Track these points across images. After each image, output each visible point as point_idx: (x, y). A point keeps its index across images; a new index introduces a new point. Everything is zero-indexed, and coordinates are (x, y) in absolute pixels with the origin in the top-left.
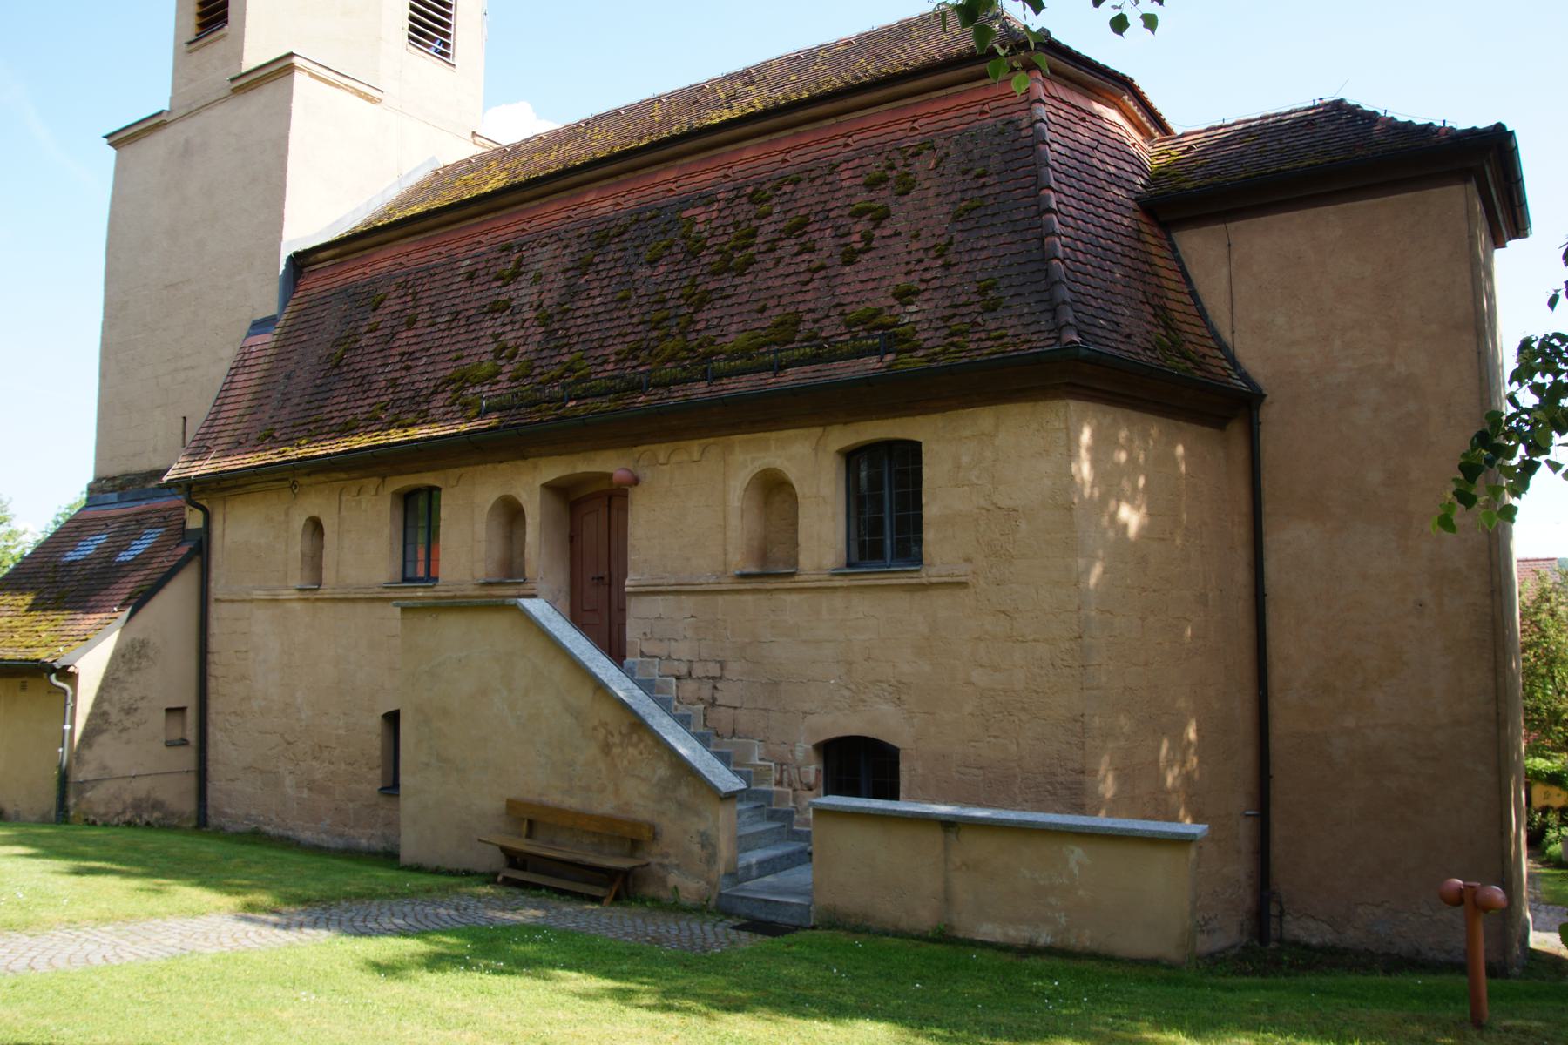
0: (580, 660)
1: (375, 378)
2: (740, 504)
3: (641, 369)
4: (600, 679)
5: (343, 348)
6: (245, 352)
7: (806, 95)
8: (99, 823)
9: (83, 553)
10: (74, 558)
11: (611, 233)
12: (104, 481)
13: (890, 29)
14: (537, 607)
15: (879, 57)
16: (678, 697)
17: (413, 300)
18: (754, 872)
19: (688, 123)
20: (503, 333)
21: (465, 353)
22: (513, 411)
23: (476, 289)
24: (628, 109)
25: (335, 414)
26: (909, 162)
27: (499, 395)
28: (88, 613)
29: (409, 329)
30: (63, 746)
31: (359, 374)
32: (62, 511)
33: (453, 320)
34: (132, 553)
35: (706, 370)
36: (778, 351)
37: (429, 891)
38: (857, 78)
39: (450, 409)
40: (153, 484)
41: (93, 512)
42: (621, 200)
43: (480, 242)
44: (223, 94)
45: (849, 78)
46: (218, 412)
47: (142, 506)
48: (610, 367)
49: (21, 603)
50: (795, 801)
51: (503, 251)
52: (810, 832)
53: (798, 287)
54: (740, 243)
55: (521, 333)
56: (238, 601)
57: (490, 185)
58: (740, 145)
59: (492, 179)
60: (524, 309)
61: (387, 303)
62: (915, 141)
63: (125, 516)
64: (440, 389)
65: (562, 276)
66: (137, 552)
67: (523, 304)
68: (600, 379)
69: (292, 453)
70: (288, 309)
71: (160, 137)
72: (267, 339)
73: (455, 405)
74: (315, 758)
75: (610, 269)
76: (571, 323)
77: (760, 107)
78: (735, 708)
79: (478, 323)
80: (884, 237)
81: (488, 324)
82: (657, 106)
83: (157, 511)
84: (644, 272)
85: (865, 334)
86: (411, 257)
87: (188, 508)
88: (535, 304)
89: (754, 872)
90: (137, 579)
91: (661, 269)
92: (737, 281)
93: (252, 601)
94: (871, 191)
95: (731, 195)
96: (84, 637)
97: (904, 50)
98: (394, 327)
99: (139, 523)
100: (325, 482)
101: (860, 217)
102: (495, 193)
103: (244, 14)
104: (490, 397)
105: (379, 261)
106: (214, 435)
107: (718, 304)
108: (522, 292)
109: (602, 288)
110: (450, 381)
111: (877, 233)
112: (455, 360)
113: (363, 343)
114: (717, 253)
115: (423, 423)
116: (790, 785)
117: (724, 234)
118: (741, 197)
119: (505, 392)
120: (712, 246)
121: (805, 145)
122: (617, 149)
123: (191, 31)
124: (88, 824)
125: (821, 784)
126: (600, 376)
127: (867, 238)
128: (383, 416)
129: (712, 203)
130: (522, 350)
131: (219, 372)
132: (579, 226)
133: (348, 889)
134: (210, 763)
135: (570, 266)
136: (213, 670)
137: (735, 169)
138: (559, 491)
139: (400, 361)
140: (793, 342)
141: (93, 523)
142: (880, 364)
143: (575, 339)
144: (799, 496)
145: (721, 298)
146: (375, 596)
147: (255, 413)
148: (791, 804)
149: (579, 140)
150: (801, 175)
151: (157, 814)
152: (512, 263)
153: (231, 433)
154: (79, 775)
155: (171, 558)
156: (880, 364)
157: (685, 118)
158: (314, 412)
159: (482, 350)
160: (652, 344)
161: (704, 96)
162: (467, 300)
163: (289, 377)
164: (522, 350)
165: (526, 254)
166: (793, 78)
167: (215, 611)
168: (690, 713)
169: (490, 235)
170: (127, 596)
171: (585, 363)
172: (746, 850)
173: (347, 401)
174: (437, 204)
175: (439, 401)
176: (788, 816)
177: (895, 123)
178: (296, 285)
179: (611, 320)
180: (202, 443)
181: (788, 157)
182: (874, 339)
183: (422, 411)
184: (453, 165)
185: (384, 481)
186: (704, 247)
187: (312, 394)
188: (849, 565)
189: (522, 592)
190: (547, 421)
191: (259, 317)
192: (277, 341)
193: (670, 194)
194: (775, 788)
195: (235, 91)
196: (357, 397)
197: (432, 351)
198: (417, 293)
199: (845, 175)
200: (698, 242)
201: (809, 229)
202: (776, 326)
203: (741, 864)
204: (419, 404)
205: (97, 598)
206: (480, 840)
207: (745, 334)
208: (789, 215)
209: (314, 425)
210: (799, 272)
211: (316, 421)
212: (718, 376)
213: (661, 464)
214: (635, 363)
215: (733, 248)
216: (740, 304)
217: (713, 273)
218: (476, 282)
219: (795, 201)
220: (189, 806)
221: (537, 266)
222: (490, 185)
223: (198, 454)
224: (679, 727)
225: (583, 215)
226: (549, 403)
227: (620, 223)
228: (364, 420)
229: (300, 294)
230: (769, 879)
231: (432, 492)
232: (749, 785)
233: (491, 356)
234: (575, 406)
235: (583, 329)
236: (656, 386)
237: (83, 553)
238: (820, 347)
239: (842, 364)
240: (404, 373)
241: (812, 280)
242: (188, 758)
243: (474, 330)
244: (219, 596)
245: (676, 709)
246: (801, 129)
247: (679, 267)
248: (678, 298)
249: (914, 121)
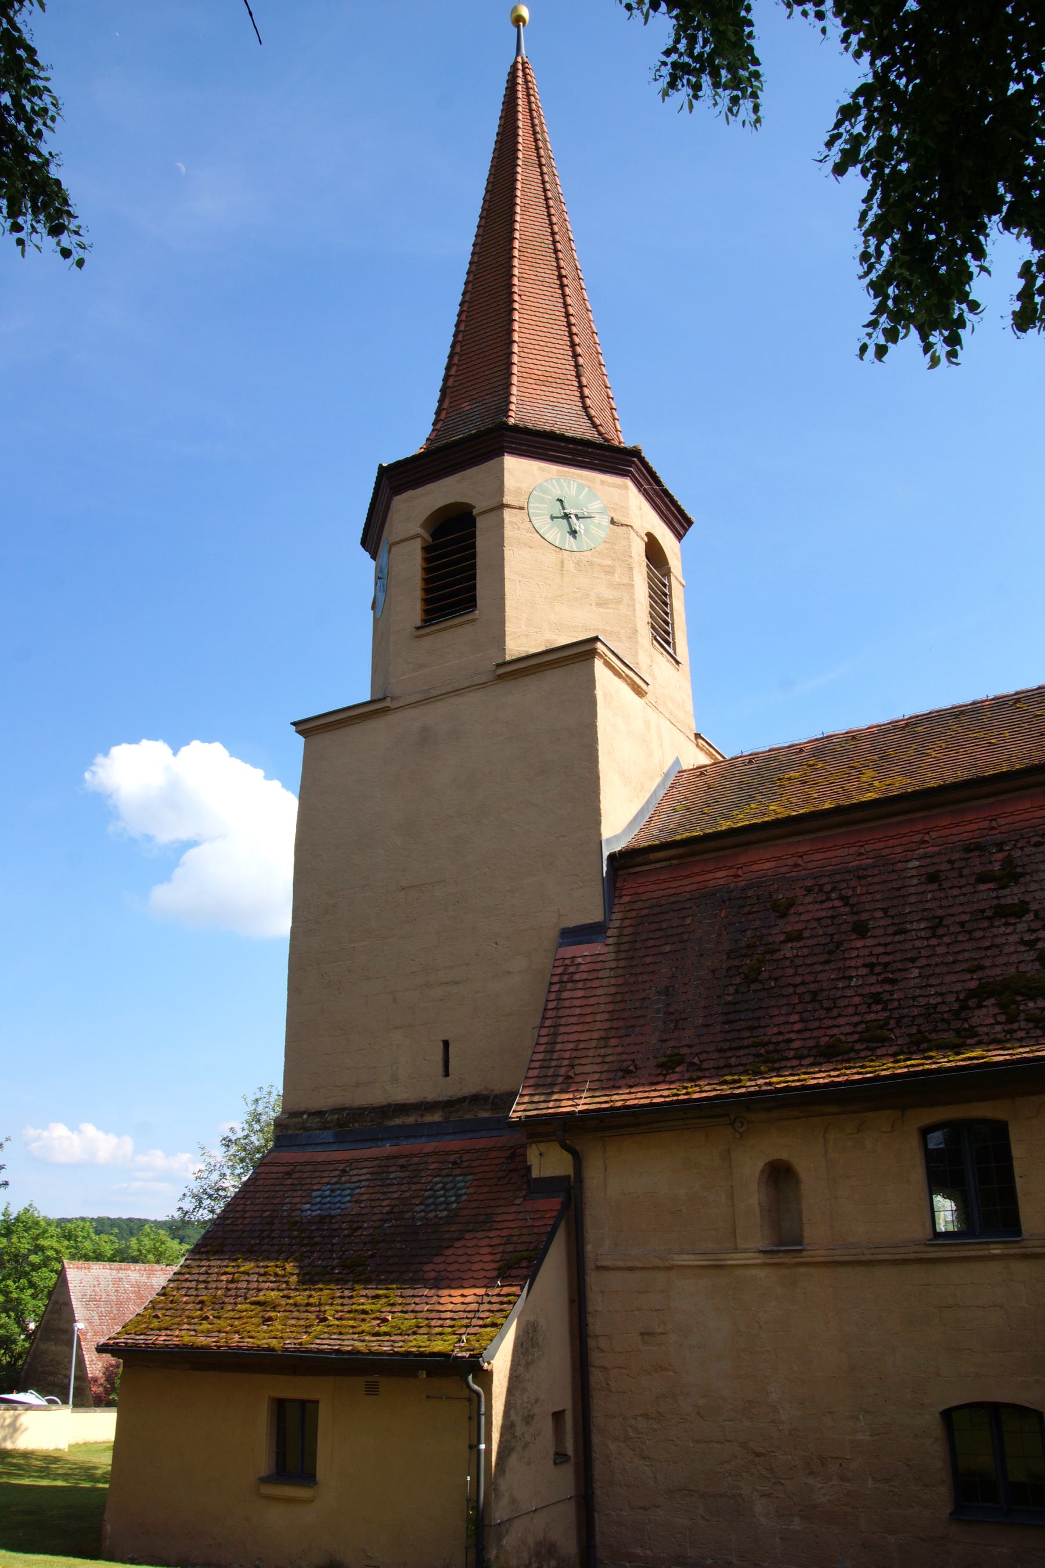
12: (305, 1116)
44: (484, 679)
74: (811, 1473)
100: (797, 1118)
146: (912, 1256)
167: (593, 1279)
195: (501, 677)
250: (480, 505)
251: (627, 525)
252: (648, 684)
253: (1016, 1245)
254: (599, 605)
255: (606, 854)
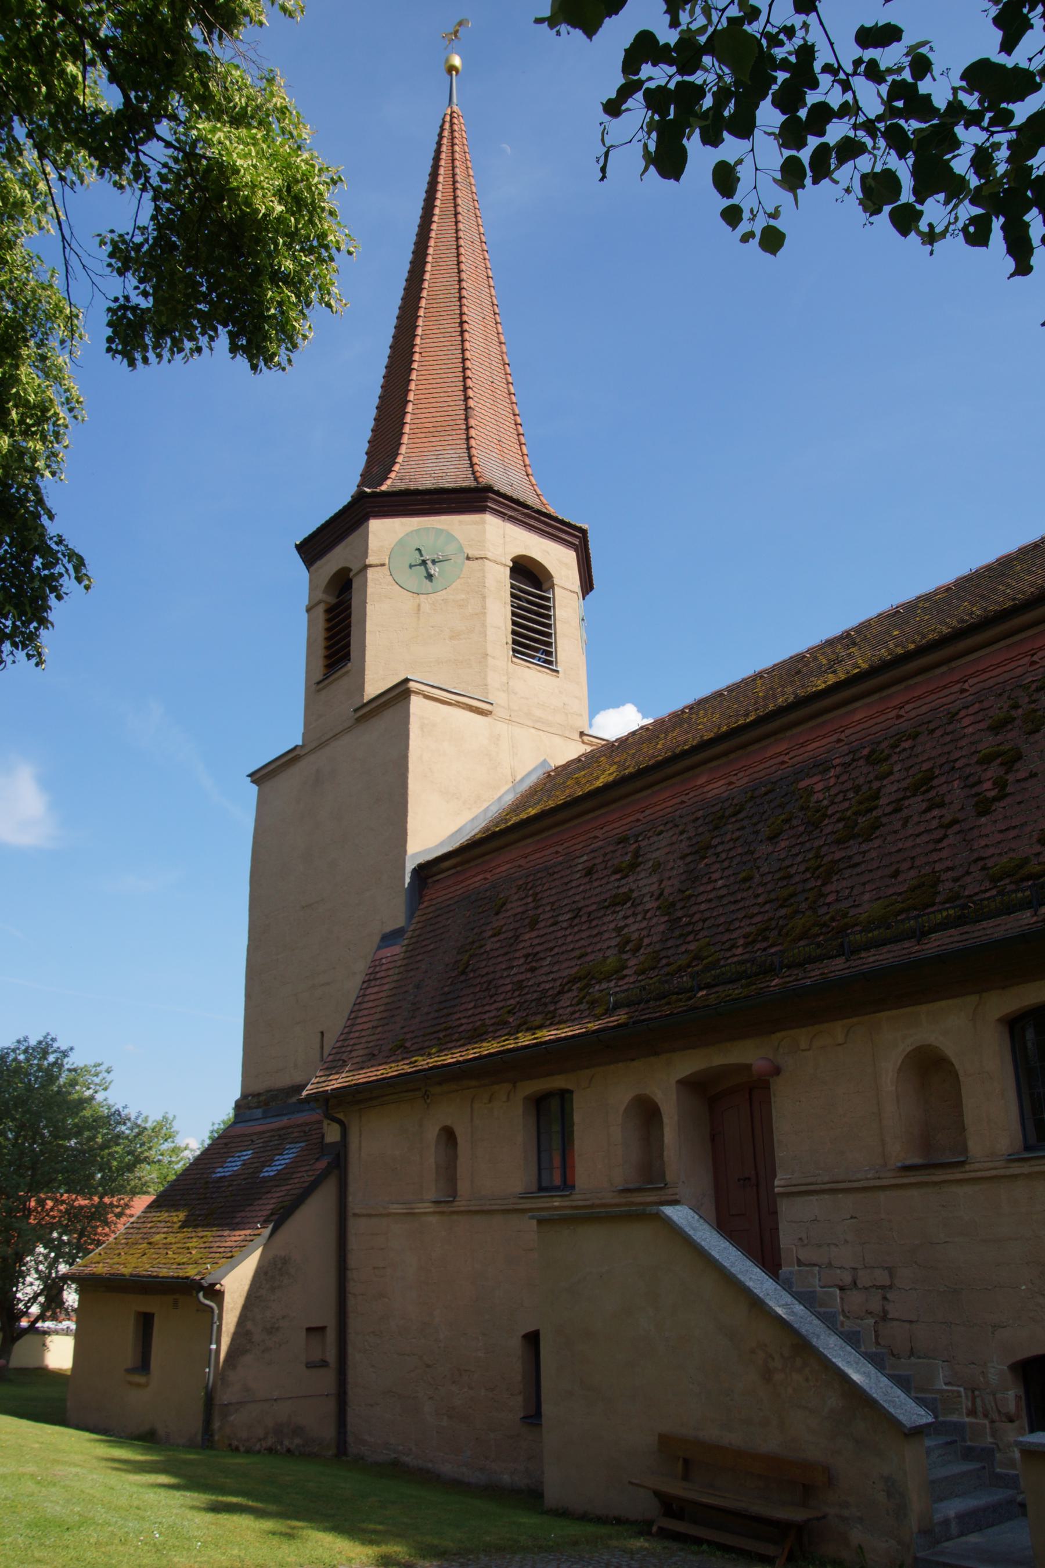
0: (731, 1273)
1: (501, 982)
2: (894, 1088)
3: (773, 950)
4: (755, 1294)
5: (468, 954)
6: (376, 964)
7: (912, 646)
8: (242, 1449)
9: (231, 1169)
10: (223, 1174)
11: (727, 814)
13: (989, 568)
14: (679, 1214)
15: (982, 597)
16: (843, 1311)
17: (533, 901)
18: (954, 1529)
19: (794, 693)
20: (626, 926)
21: (589, 950)
22: (642, 1006)
23: (596, 884)
24: (731, 689)
25: (464, 1021)
26: (1033, 698)
27: (626, 990)
28: (234, 1230)
29: (532, 930)
30: (209, 1367)
31: (485, 979)
32: (216, 1127)
33: (575, 917)
34: (275, 1168)
35: (842, 945)
36: (919, 916)
37: (575, 1544)
38: (963, 621)
39: (577, 1008)
40: (294, 1100)
41: (241, 1129)
42: (733, 779)
43: (596, 837)
45: (955, 623)
46: (353, 1025)
47: (284, 1121)
48: (740, 951)
49: (175, 1219)
50: (993, 1435)
51: (619, 843)
52: (1017, 1475)
53: (931, 847)
54: (862, 807)
55: (644, 924)
56: (376, 1215)
57: (601, 780)
58: (850, 707)
59: (603, 774)
60: (645, 900)
61: (508, 906)
62: (1037, 675)
63: (268, 1131)
64: (566, 988)
65: (680, 862)
66: (280, 1168)
67: (644, 895)
68: (730, 964)
69: (424, 1062)
70: (415, 920)
71: (295, 770)
72: (396, 950)
73: (582, 1003)
74: (454, 1382)
75: (730, 849)
76: (694, 909)
77: (865, 666)
78: (911, 1322)
79: (600, 918)
80: (1018, 781)
81: (610, 918)
82: (759, 682)
83: (298, 1126)
84: (764, 849)
85: (1013, 887)
86: (529, 859)
87: (326, 1122)
88: (656, 894)
89: (954, 1529)
90: (278, 1195)
91: (783, 844)
92: (864, 847)
93: (389, 1215)
94: (997, 734)
95: (847, 759)
96: (229, 1255)
97: (1008, 586)
98: (516, 929)
99: (280, 1139)
101: (989, 763)
102: (607, 787)
103: (364, 650)
104: (616, 993)
105: (499, 866)
106: (349, 1048)
107: (847, 873)
108: (641, 883)
109: (723, 870)
110: (574, 980)
111: (1011, 777)
112: (579, 958)
113: (488, 948)
114: (839, 820)
115: (551, 1024)
116: (986, 1416)
117: (845, 800)
118: (858, 760)
119: (632, 986)
120: (833, 814)
121: (919, 698)
122: (724, 729)
123: (318, 674)
124: (232, 1450)
125: (1024, 1413)
126: (729, 961)
127: (1000, 784)
128: (511, 1020)
129: (828, 769)
130: (646, 941)
131: (352, 986)
132: (694, 810)
133: (488, 1538)
134: (349, 1387)
135: (688, 851)
136: (352, 1287)
137: (848, 732)
138: (693, 1085)
139: (525, 963)
140: (934, 904)
141: (239, 1140)
142: (1035, 919)
143: (700, 925)
144: (961, 1073)
145: (850, 867)
146: (511, 1207)
147: (387, 1024)
148: (990, 1439)
149: (685, 726)
150: (919, 729)
151: (297, 1441)
152: (630, 855)
153: (366, 1045)
154: (225, 1397)
155: (310, 1173)
156: (1035, 919)
157: (789, 689)
158: (443, 1020)
159: (605, 945)
160: (781, 923)
161: (806, 665)
162: (587, 896)
163: (418, 987)
164: (646, 941)
165: (643, 844)
166: (895, 633)
167: (356, 1227)
168: (858, 1329)
169: (605, 829)
170: (270, 1212)
171: (713, 949)
172: (941, 1500)
173: (475, 1007)
174: (551, 804)
175: (566, 1000)
176: (986, 1455)
177: (1012, 660)
178: (421, 897)
179: (735, 902)
180: (338, 1057)
181: (902, 712)
182: (1023, 891)
183: (550, 1012)
184: (564, 766)
185: (515, 1087)
186: (825, 816)
187: (441, 1002)
188: (1027, 1148)
189: (664, 1198)
190: (678, 1013)
191: (389, 928)
192: (406, 952)
193: (783, 767)
194: (967, 1420)
195: (359, 720)
196: (484, 1002)
197: (556, 950)
198: (537, 894)
199: (966, 722)
200: (818, 811)
201: (935, 783)
202: (913, 889)
203: (938, 1517)
204: (545, 1005)
205: (242, 1214)
206: (631, 1483)
207: (880, 901)
208: (911, 772)
209: (444, 1033)
210: (931, 830)
211: (446, 1029)
212: (855, 950)
213: (803, 1050)
214: (765, 944)
215: (855, 813)
216: (871, 871)
217: (838, 842)
218: (595, 877)
219: (916, 756)
220: (329, 1433)
221: (654, 855)
222: (601, 780)
223: (334, 1067)
224: (849, 1348)
225: (696, 799)
226: (678, 994)
227: (735, 801)
228: (492, 1025)
229: (426, 904)
230: (973, 1539)
231: (564, 1096)
232: (936, 1417)
233: (615, 951)
234: (706, 995)
235: (707, 914)
236: (789, 967)
237: (231, 1169)
238: (965, 906)
239: (991, 923)
240: (529, 975)
241: (945, 836)
242: (327, 1380)
243: (597, 925)
244: (357, 1211)
245: (842, 1324)
246: (911, 682)
247: (801, 840)
248: (804, 872)
249: (1033, 655)
250: (355, 567)
251: (482, 558)
252: (492, 704)
253: (567, 1199)
254: (451, 638)
255: (410, 866)
